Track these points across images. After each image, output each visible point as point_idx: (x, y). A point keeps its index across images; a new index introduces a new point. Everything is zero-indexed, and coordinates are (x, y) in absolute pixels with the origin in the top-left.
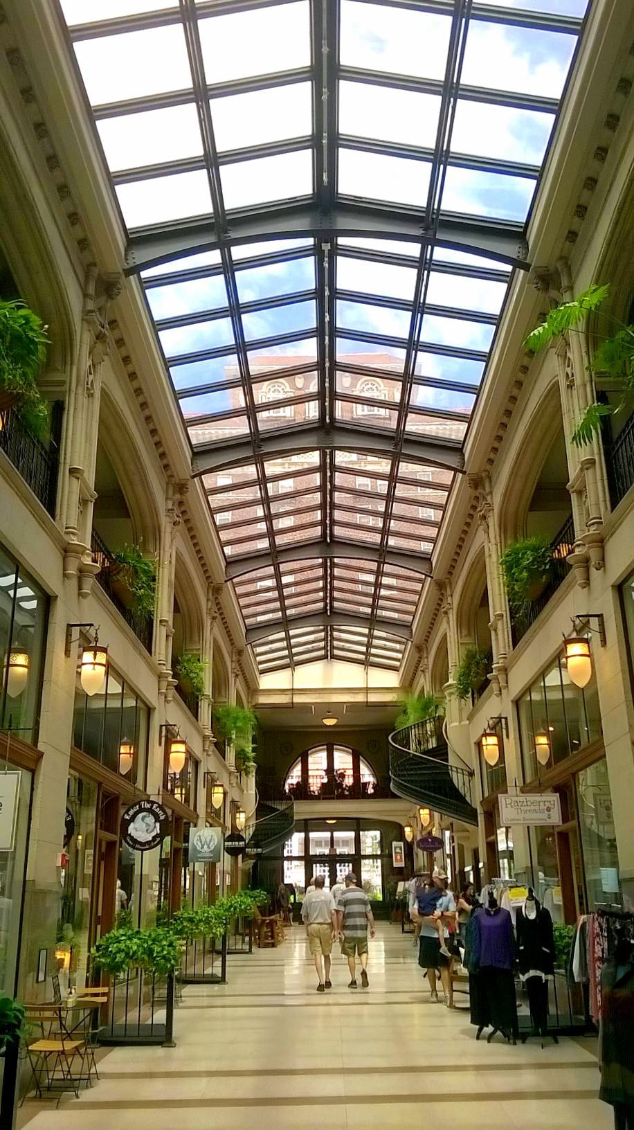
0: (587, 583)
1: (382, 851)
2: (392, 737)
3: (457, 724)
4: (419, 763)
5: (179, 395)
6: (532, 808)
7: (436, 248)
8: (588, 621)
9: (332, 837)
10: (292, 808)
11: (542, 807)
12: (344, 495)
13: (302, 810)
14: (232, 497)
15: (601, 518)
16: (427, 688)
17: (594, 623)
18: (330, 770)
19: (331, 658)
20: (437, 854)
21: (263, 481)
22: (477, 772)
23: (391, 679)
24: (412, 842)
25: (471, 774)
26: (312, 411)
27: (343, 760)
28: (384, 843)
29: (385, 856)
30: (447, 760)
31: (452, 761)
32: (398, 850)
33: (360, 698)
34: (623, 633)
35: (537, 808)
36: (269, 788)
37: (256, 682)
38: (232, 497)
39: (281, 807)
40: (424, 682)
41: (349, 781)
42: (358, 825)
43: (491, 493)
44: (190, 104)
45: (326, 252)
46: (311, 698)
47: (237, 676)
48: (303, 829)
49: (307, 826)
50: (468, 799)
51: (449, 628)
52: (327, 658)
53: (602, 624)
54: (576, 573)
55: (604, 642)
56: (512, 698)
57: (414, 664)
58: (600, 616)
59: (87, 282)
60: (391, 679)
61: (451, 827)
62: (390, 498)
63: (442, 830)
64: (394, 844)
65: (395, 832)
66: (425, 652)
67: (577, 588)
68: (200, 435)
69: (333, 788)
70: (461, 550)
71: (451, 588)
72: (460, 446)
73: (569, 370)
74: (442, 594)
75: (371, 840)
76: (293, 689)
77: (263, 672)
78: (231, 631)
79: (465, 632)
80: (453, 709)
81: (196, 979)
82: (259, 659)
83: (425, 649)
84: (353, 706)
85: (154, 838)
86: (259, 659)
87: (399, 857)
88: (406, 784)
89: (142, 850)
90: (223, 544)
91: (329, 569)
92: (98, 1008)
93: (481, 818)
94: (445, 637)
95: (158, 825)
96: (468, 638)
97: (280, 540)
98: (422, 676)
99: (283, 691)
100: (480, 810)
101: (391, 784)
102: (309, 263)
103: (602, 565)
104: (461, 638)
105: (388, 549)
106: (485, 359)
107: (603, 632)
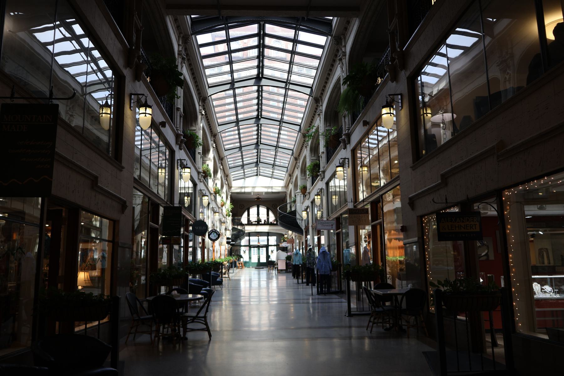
2: (279, 208)
6: (327, 224)
7: (300, 32)
9: (259, 239)
10: (244, 228)
11: (330, 224)
21: (228, 41)
23: (282, 183)
30: (296, 216)
35: (328, 225)
40: (291, 186)
42: (268, 234)
44: (247, 222)
45: (262, 25)
47: (183, 59)
49: (250, 234)
51: (306, 152)
55: (349, 166)
57: (299, 151)
58: (348, 159)
59: (199, 101)
62: (291, 63)
66: (298, 160)
70: (318, 107)
74: (317, 106)
75: (273, 240)
78: (212, 127)
79: (303, 175)
83: (321, 100)
85: (216, 238)
88: (392, 24)
91: (260, 93)
92: (370, 234)
93: (304, 233)
94: (305, 157)
95: (217, 235)
97: (236, 76)
98: (306, 149)
100: (304, 231)
104: (312, 157)
105: (291, 82)
106: (320, 59)
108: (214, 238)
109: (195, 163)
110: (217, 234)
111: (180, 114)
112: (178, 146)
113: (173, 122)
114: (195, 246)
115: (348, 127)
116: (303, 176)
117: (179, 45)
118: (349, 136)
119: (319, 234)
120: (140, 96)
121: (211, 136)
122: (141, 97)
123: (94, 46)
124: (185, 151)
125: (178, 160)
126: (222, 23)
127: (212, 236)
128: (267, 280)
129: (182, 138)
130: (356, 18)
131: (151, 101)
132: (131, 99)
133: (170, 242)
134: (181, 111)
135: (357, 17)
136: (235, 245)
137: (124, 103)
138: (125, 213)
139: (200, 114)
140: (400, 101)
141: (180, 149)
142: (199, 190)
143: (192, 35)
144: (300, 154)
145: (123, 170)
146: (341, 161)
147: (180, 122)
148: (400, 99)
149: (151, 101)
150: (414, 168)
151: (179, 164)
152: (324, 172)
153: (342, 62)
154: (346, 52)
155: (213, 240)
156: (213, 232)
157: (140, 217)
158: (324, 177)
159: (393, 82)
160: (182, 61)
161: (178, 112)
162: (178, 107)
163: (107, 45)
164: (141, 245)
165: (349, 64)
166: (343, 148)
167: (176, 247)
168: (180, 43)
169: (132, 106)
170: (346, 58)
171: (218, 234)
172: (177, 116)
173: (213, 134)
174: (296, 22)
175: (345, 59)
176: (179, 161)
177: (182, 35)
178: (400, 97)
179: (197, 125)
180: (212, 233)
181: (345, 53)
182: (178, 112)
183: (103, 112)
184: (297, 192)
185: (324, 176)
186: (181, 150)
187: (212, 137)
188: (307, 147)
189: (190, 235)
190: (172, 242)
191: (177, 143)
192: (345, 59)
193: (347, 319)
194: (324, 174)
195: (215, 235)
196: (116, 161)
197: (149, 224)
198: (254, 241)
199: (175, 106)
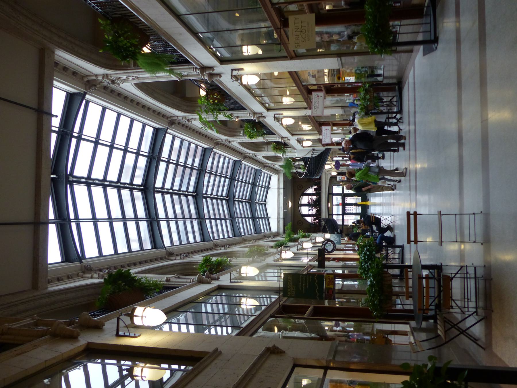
0: (219, 75)
3: (296, 154)
4: (309, 169)
6: (317, 103)
8: (234, 75)
10: (323, 219)
13: (324, 215)
15: (194, 68)
16: (280, 164)
17: (235, 73)
18: (308, 205)
19: (265, 202)
20: (341, 163)
22: (313, 148)
23: (275, 179)
24: (337, 172)
25: (314, 150)
26: (138, 194)
27: (305, 200)
30: (309, 158)
31: (309, 156)
32: (340, 178)
33: (282, 191)
36: (316, 228)
37: (275, 233)
39: (323, 223)
40: (277, 165)
41: (314, 198)
42: (331, 194)
43: (222, 139)
46: (281, 211)
48: (332, 216)
49: (331, 214)
50: (322, 151)
54: (261, 119)
56: (220, 65)
58: (232, 70)
59: (171, 259)
60: (275, 179)
61: (332, 158)
63: (333, 161)
64: (338, 180)
65: (333, 180)
69: (317, 204)
71: (218, 139)
72: (204, 149)
73: (131, 78)
75: (337, 189)
76: (278, 218)
79: (263, 149)
80: (289, 154)
82: (266, 231)
84: (285, 195)
85: (332, 244)
86: (266, 231)
87: (343, 178)
89: (336, 247)
90: (229, 237)
94: (264, 157)
95: (329, 243)
96: (266, 148)
99: (278, 222)
101: (316, 178)
102: (76, 187)
103: (211, 68)
111: (176, 278)
112: (213, 282)
113: (178, 286)
115: (192, 70)
116: (264, 149)
117: (92, 278)
118: (203, 68)
121: (215, 250)
123: (185, 366)
124: (222, 275)
126: (68, 226)
127: (330, 249)
128: (382, 196)
129: (205, 276)
130: (55, 55)
132: (124, 336)
133: (332, 293)
134: (170, 277)
135: (53, 52)
136: (341, 229)
138: (284, 350)
139: (185, 259)
141: (218, 279)
143: (82, 262)
144: (240, 152)
145: (219, 350)
151: (236, 281)
152: (282, 138)
153: (116, 80)
154: (103, 74)
157: (308, 333)
158: (261, 113)
161: (171, 280)
162: (165, 280)
163: (22, 368)
164: (339, 331)
165: (116, 70)
166: (220, 78)
168: (90, 276)
170: (111, 74)
171: (327, 241)
172: (176, 282)
173: (214, 248)
174: (69, 136)
175: (112, 76)
177: (81, 274)
179: (198, 262)
181: (104, 76)
183: (140, 375)
184: (282, 157)
185: (260, 113)
186: (219, 278)
187: (216, 249)
191: (209, 283)
192: (112, 76)
194: (256, 113)
195: (329, 246)
197: (307, 317)
198: (338, 210)
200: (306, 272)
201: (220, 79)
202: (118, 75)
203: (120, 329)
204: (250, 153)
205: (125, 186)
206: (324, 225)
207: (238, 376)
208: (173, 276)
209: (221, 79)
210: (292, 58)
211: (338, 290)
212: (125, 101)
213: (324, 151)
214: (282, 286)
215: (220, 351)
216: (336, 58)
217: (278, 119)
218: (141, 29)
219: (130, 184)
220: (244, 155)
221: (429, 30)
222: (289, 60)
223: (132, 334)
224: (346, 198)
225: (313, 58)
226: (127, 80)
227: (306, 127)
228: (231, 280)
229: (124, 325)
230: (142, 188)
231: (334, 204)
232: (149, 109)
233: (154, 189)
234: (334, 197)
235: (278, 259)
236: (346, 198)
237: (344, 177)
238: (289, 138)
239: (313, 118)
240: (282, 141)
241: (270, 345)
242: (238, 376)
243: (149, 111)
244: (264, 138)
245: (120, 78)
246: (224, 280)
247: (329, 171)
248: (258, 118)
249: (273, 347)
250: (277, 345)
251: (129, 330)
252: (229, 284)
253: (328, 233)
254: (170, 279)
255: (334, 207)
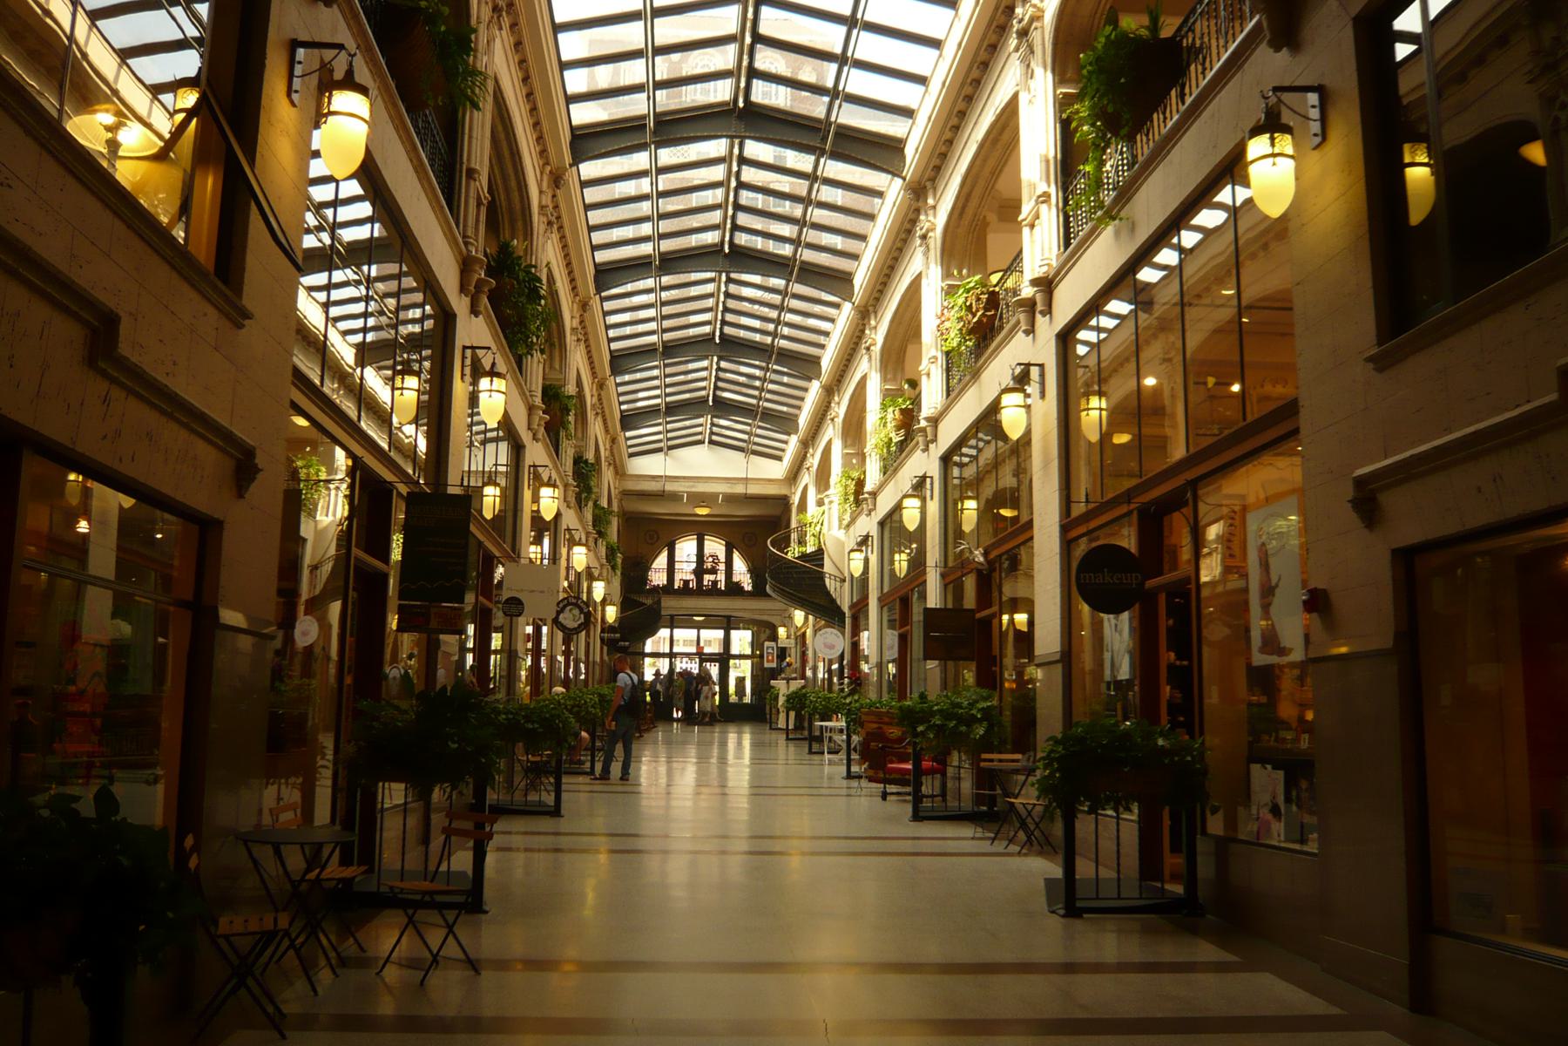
0: (1031, 331)
1: (753, 651)
4: (792, 567)
5: (564, 66)
10: (659, 602)
12: (751, 195)
14: (604, 76)
17: (1034, 372)
25: (844, 581)
28: (756, 644)
29: (757, 656)
30: (822, 566)
31: (828, 567)
33: (739, 489)
34: (1410, 63)
38: (604, 76)
49: (673, 623)
50: (839, 603)
51: (867, 368)
52: (703, 442)
53: (1042, 375)
55: (1043, 395)
58: (1041, 366)
59: (542, 180)
64: (767, 644)
67: (919, 452)
68: (584, 114)
71: (876, 317)
75: (741, 640)
77: (631, 455)
81: (527, 808)
85: (580, 625)
93: (848, 621)
95: (582, 616)
103: (1048, 310)
107: (1042, 383)
108: (571, 624)
109: (521, 373)
110: (581, 611)
112: (466, 301)
114: (513, 648)
118: (1047, 285)
119: (907, 625)
120: (328, 54)
122: (333, 56)
124: (490, 324)
125: (465, 348)
131: (363, 74)
136: (630, 650)
137: (263, 65)
138: (246, 496)
140: (1315, 114)
141: (474, 311)
142: (530, 466)
145: (247, 322)
146: (1018, 370)
147: (477, 221)
148: (1313, 107)
149: (363, 74)
150: (1381, 362)
151: (468, 362)
155: (569, 629)
156: (569, 604)
158: (934, 440)
159: (1278, 49)
160: (492, 17)
161: (472, 183)
162: (473, 166)
167: (449, 640)
169: (294, 88)
176: (469, 352)
178: (1313, 98)
180: (565, 607)
182: (472, 183)
185: (936, 436)
188: (872, 348)
189: (495, 610)
190: (434, 624)
191: (463, 289)
193: (1055, 923)
196: (220, 285)
197: (353, 556)
198: (709, 643)
199: (462, 163)
200: (497, 554)
201: (1020, 333)
202: (1040, 47)
203: (316, 51)
204: (840, 409)
205: (745, 57)
206: (644, 604)
207: (167, 374)
208: (486, 191)
209: (1021, 335)
210: (1065, 529)
211: (438, 640)
212: (976, 65)
213: (839, 608)
214: (451, 490)
215: (244, 326)
216: (1059, 649)
217: (920, 485)
218: (1152, 121)
219: (751, 67)
220: (835, 388)
221: (1122, 896)
222: (1060, 521)
223: (297, 83)
224: (717, 664)
225: (1062, 585)
226: (1027, 73)
227: (901, 562)
228: (473, 348)
229: (327, 60)
230: (741, 104)
231: (703, 632)
232: (956, 129)
233: (736, 137)
234: (720, 634)
235: (537, 477)
236: (717, 664)
237: (773, 661)
238: (873, 513)
239: (921, 580)
240: (866, 496)
241: (260, 460)
242: (167, 374)
243: (950, 130)
244: (1046, 195)
245: (1032, 52)
246: (474, 330)
247: (788, 621)
248: (923, 430)
249: (256, 466)
250: (259, 476)
251: (314, 75)
252: (459, 344)
253: (622, 613)
254: (475, 180)
255: (694, 632)
